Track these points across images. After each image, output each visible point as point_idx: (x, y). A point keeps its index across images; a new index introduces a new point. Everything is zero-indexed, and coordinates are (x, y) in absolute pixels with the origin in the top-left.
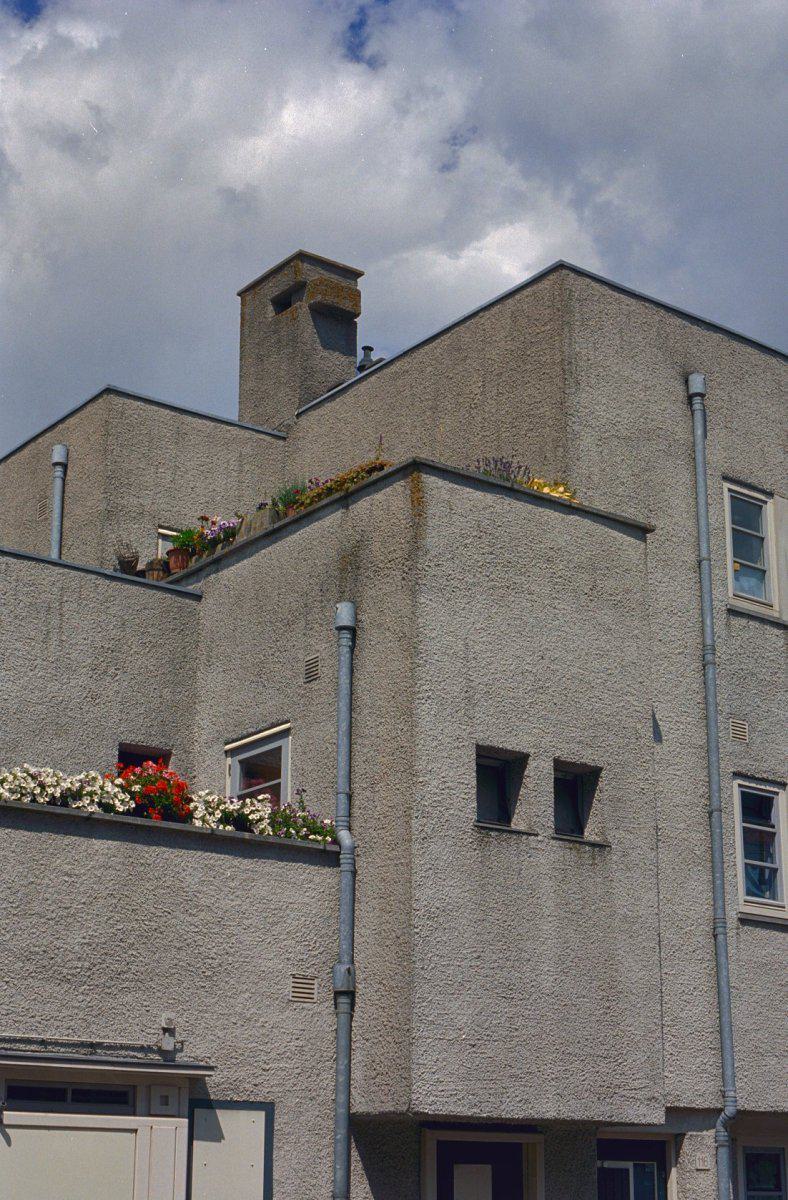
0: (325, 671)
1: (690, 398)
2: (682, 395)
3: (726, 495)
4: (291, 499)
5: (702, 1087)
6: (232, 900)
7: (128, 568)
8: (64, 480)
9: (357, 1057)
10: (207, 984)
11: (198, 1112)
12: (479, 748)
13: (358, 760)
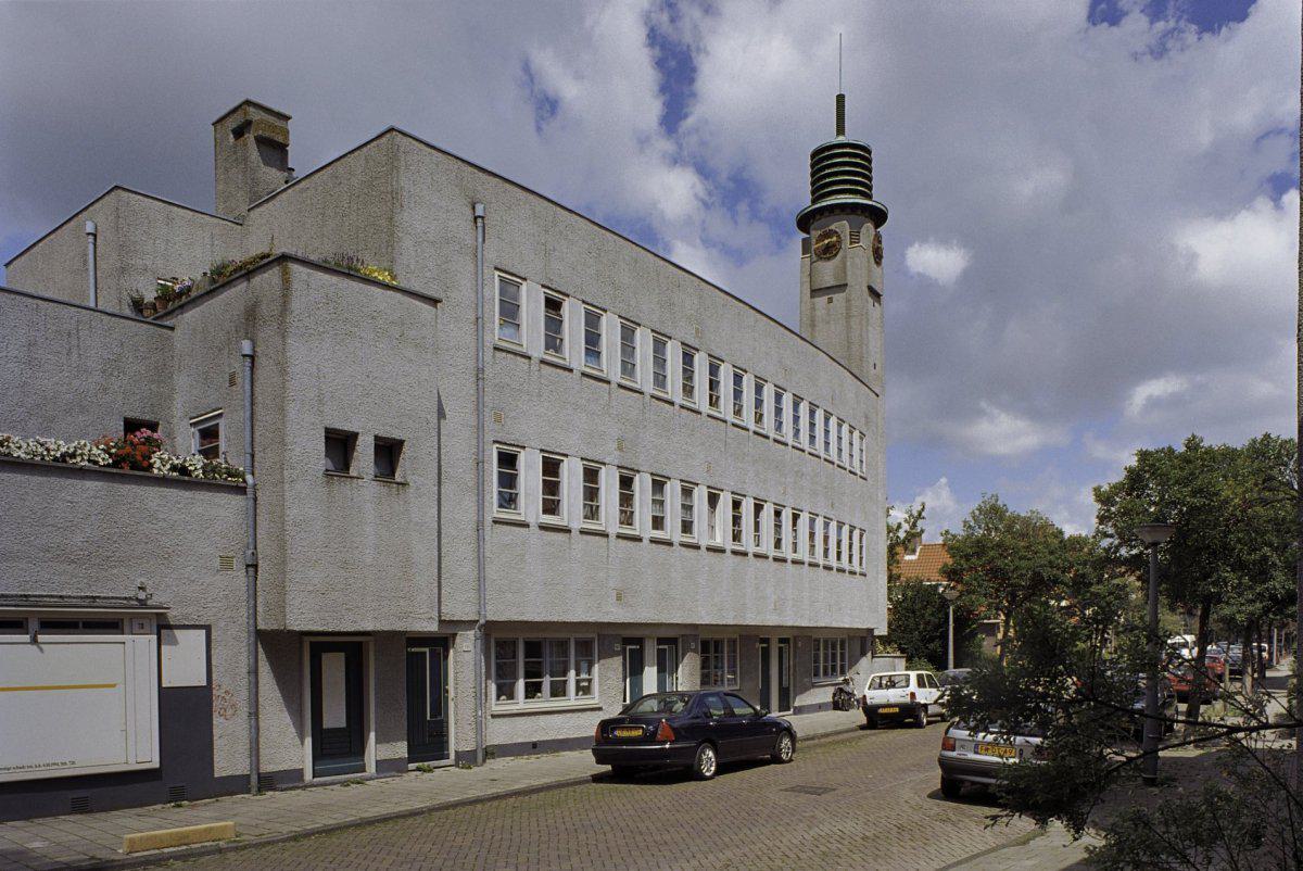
0: (239, 380)
1: (476, 218)
2: (471, 218)
3: (497, 280)
4: (219, 271)
7: (138, 305)
8: (95, 245)
9: (260, 600)
10: (165, 562)
12: (328, 431)
13: (257, 434)
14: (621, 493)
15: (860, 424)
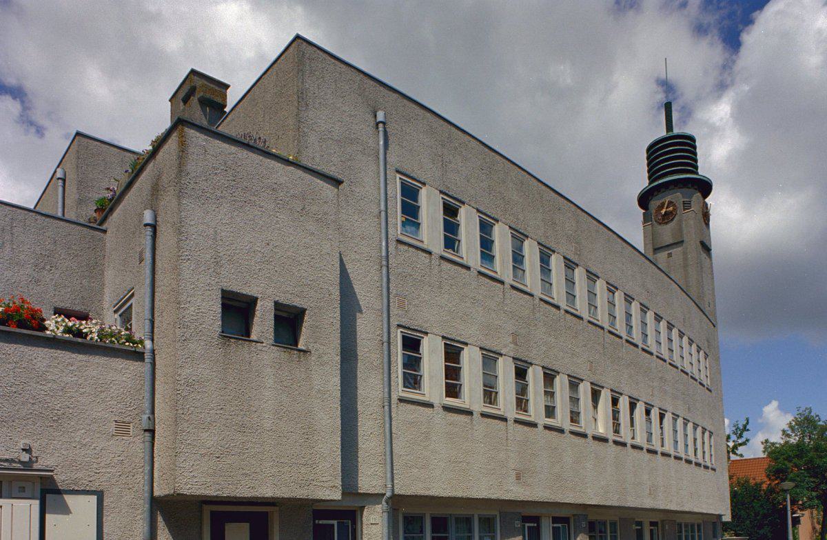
1: (377, 124)
2: (373, 123)
5: (374, 483)
6: (72, 378)
10: (55, 425)
11: (49, 497)
14: (517, 398)
15: (704, 346)
